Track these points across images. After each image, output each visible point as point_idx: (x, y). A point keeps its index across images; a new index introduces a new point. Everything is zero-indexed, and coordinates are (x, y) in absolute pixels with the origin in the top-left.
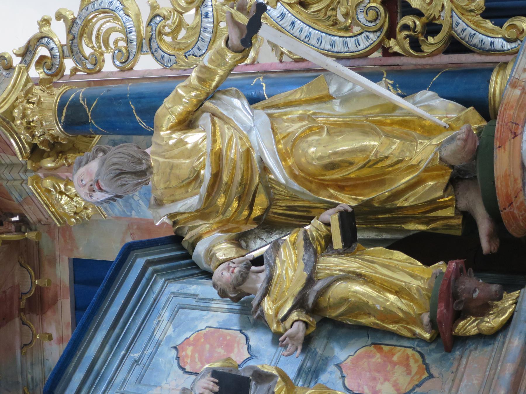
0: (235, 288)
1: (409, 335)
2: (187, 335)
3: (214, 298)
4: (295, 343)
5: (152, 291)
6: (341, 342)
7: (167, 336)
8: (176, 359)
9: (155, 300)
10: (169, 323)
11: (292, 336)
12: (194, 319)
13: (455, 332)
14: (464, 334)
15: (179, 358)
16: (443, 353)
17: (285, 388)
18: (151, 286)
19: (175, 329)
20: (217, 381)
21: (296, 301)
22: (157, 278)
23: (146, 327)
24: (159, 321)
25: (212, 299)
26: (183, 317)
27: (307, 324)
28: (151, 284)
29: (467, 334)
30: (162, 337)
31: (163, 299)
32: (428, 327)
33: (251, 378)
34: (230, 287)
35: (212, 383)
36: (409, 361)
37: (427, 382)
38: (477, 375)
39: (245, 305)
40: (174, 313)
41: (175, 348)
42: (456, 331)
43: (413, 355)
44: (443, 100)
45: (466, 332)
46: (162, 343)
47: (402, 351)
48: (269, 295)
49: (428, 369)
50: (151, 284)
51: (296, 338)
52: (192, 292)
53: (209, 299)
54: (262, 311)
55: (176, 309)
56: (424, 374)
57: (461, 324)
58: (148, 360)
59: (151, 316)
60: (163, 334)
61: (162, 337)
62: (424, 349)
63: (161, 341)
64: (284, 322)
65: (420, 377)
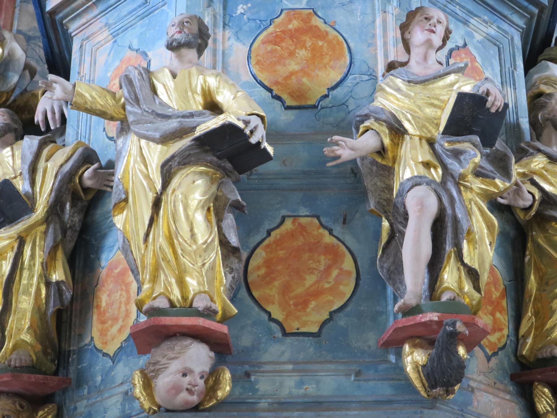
0: (547, 120)
1: (523, 330)
2: (478, 59)
3: (517, 91)
4: (511, 196)
5: (513, 13)
6: (500, 249)
7: (472, 33)
8: (456, 46)
9: (505, 17)
10: (485, 35)
11: (520, 193)
12: (492, 65)
13: (537, 385)
14: (537, 396)
15: (458, 49)
16: (509, 372)
17: (496, 191)
18: (519, 12)
19: (480, 43)
20: (500, 110)
21: (553, 196)
22: (525, 19)
23: (480, 7)
24: (487, 23)
25: (516, 89)
26: (492, 52)
27: (527, 209)
28: (521, 11)
29: (536, 400)
30: (472, 26)
31: (506, 26)
32: (548, 354)
33: (494, 148)
34: (549, 114)
35: (499, 105)
36: (498, 332)
37: (484, 354)
38: (501, 414)
39: (516, 129)
40: (494, 41)
41: (465, 45)
42: (540, 387)
43: (503, 336)
44: (2, 283)
45: (539, 398)
46: (466, 27)
47: (504, 322)
48: (549, 162)
49: (495, 354)
50: (521, 11)
51: (517, 197)
52: (517, 63)
53: (514, 85)
54: (532, 154)
55: (498, 43)
56: (490, 350)
57: (546, 390)
58: (450, 11)
59: (491, 14)
60: (475, 28)
61: (472, 26)
62: (510, 349)
63: (468, 26)
64: (529, 182)
65: (487, 346)
